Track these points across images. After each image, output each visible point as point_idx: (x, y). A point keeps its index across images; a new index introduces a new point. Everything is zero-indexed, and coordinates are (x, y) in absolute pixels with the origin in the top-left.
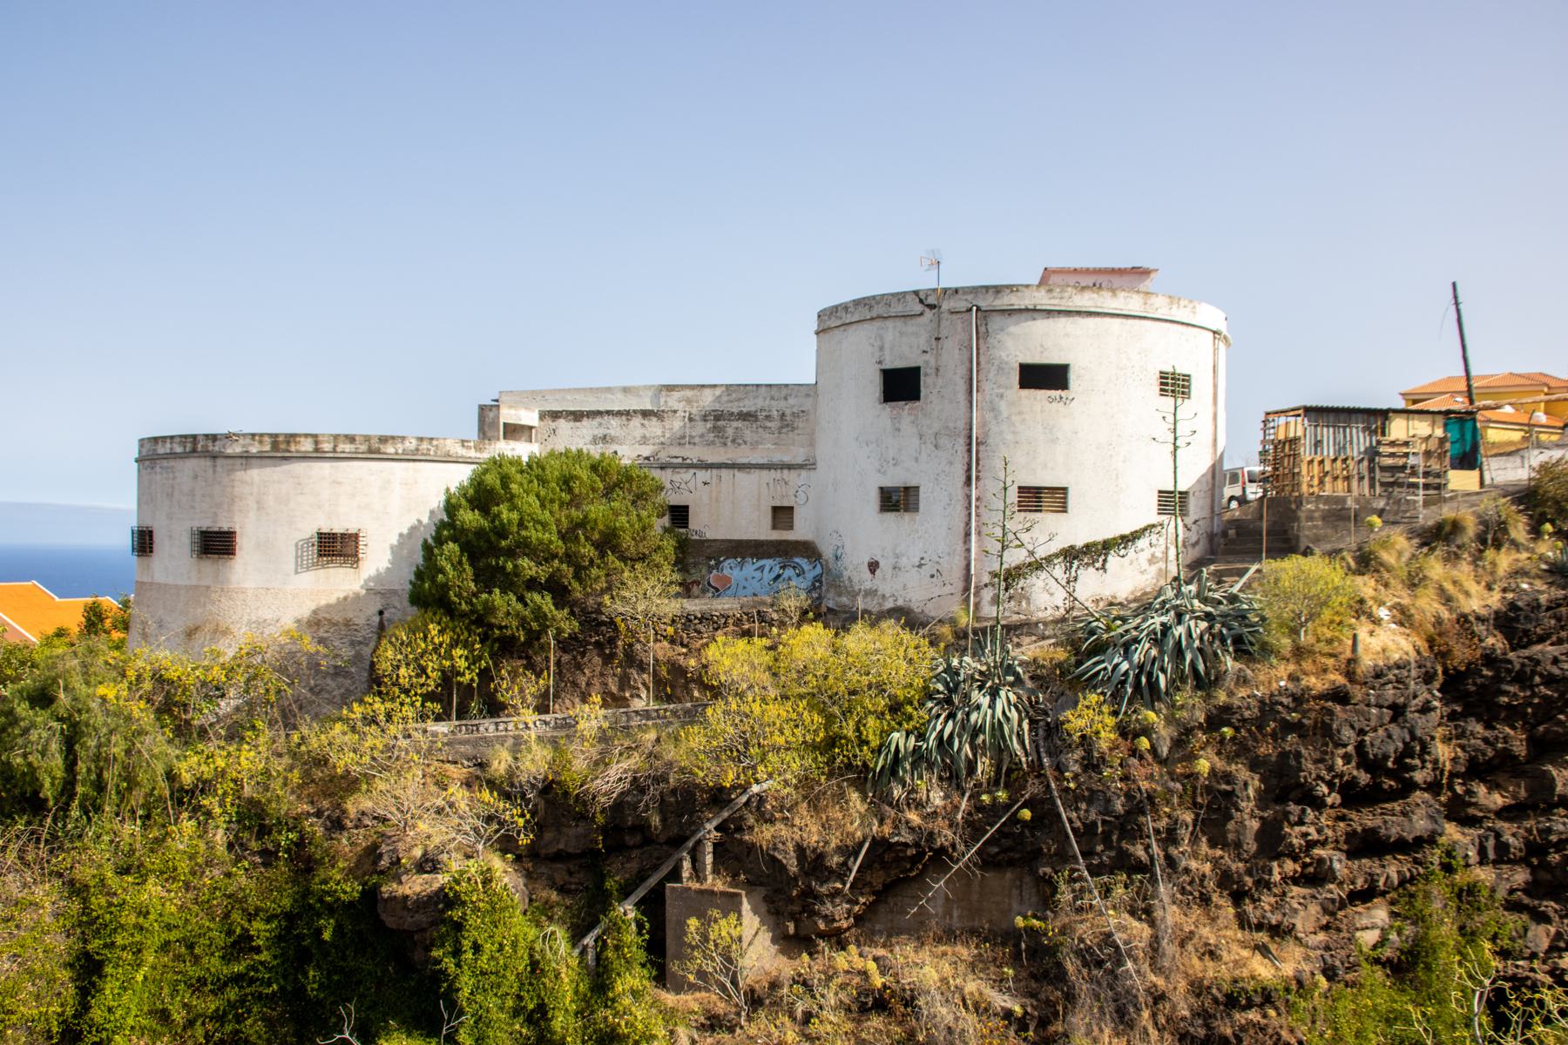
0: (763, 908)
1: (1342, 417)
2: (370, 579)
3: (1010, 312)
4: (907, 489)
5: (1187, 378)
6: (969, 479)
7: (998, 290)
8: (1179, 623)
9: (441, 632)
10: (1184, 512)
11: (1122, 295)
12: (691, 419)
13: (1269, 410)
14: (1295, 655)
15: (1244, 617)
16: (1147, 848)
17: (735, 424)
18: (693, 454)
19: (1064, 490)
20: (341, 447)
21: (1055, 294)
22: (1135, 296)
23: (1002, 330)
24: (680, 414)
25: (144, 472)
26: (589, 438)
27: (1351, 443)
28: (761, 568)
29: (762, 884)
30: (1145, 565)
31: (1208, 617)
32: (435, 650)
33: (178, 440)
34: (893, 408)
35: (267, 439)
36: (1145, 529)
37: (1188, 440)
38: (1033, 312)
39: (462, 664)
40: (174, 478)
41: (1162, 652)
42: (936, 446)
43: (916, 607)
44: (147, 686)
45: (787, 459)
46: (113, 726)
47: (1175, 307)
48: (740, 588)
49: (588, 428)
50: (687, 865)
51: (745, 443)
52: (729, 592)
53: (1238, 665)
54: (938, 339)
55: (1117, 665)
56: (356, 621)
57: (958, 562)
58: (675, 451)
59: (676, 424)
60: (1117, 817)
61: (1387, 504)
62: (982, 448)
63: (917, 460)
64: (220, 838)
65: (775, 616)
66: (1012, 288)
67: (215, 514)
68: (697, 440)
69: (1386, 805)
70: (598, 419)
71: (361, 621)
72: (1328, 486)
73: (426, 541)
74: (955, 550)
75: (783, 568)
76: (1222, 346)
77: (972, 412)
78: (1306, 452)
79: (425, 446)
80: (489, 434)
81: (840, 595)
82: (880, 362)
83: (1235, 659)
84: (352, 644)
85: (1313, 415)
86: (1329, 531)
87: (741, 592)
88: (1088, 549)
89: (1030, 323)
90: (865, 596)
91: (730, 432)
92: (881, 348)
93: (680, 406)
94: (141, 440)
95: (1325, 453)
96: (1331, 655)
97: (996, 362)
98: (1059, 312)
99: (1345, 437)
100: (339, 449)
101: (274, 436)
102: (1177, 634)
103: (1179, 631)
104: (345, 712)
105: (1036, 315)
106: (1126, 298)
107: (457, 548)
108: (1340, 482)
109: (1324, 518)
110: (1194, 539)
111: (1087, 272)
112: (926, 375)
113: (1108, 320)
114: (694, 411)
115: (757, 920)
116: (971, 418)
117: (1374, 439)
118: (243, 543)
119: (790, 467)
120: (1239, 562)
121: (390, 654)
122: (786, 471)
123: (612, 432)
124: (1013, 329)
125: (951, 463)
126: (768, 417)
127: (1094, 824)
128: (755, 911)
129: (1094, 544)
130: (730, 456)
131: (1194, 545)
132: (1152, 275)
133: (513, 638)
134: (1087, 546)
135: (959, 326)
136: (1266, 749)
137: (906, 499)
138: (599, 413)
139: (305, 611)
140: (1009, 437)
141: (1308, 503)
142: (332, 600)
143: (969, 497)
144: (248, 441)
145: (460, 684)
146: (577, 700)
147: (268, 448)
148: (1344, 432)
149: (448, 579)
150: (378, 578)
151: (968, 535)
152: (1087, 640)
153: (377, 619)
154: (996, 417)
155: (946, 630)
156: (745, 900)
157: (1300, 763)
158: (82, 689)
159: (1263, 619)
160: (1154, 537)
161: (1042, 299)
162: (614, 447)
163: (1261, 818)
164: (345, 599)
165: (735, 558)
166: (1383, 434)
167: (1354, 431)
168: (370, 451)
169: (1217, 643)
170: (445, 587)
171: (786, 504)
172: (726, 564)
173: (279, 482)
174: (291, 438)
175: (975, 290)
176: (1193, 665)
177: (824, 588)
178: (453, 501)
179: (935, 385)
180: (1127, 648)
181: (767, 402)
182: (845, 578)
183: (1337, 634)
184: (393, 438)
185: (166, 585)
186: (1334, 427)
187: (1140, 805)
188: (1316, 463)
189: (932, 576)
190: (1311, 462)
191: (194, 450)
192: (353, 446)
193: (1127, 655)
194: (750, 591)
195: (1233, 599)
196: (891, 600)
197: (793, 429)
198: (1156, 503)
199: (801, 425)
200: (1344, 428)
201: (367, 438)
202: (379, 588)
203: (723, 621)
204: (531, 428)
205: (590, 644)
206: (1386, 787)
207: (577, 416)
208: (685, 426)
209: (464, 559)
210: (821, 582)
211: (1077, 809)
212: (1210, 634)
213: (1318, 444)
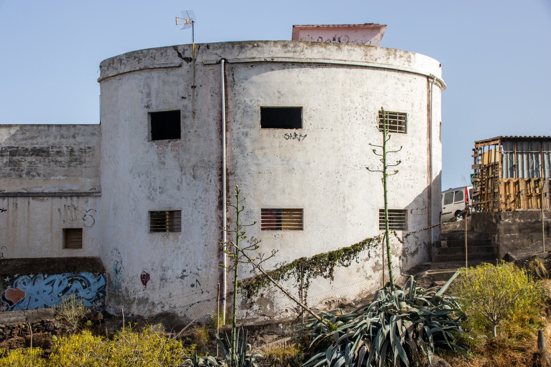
1: (534, 145)
3: (253, 64)
4: (172, 213)
5: (403, 116)
6: (221, 203)
7: (242, 45)
8: (387, 323)
10: (402, 226)
11: (346, 48)
13: (478, 140)
14: (489, 349)
15: (445, 317)
17: (29, 159)
19: (301, 211)
21: (289, 49)
22: (357, 49)
23: (246, 79)
27: (543, 167)
28: (52, 283)
30: (370, 272)
31: (413, 317)
34: (159, 145)
36: (363, 243)
37: (396, 168)
41: (373, 348)
42: (194, 177)
43: (179, 312)
45: (76, 188)
47: (392, 57)
51: (39, 175)
52: (22, 305)
53: (438, 359)
54: (194, 87)
55: (336, 359)
57: (213, 272)
62: (231, 178)
63: (179, 188)
65: (58, 325)
66: (254, 44)
72: (523, 203)
74: (210, 264)
75: (71, 281)
76: (436, 90)
77: (222, 148)
78: (503, 176)
81: (119, 303)
82: (148, 107)
83: (436, 353)
85: (508, 144)
86: (525, 241)
87: (33, 304)
88: (316, 260)
90: (138, 304)
91: (25, 165)
92: (149, 95)
95: (520, 176)
96: (522, 350)
97: (242, 106)
98: (293, 63)
99: (537, 161)
102: (385, 332)
103: (389, 328)
105: (273, 66)
106: (349, 51)
108: (533, 199)
109: (520, 230)
110: (413, 249)
111: (328, 28)
112: (185, 117)
113: (334, 69)
116: (222, 153)
119: (78, 195)
120: (449, 268)
122: (75, 199)
124: (255, 78)
125: (206, 191)
126: (58, 153)
129: (322, 256)
130: (25, 186)
131: (413, 254)
132: (383, 30)
134: (315, 258)
135: (211, 77)
137: (171, 222)
140: (253, 168)
141: (506, 217)
143: (221, 218)
148: (537, 158)
151: (221, 250)
152: (316, 337)
154: (242, 152)
155: (201, 332)
159: (464, 318)
160: (372, 251)
161: (279, 53)
165: (28, 274)
169: (420, 339)
171: (75, 226)
172: (20, 280)
175: (223, 46)
176: (400, 359)
177: (107, 298)
179: (192, 126)
180: (344, 346)
181: (58, 140)
182: (123, 289)
183: (527, 330)
186: (527, 154)
188: (512, 185)
189: (193, 286)
190: (508, 183)
193: (344, 351)
194: (41, 303)
195: (436, 300)
196: (159, 306)
197: (81, 163)
198: (379, 216)
200: (537, 155)
203: (8, 332)
210: (104, 293)
212: (415, 331)
213: (513, 168)
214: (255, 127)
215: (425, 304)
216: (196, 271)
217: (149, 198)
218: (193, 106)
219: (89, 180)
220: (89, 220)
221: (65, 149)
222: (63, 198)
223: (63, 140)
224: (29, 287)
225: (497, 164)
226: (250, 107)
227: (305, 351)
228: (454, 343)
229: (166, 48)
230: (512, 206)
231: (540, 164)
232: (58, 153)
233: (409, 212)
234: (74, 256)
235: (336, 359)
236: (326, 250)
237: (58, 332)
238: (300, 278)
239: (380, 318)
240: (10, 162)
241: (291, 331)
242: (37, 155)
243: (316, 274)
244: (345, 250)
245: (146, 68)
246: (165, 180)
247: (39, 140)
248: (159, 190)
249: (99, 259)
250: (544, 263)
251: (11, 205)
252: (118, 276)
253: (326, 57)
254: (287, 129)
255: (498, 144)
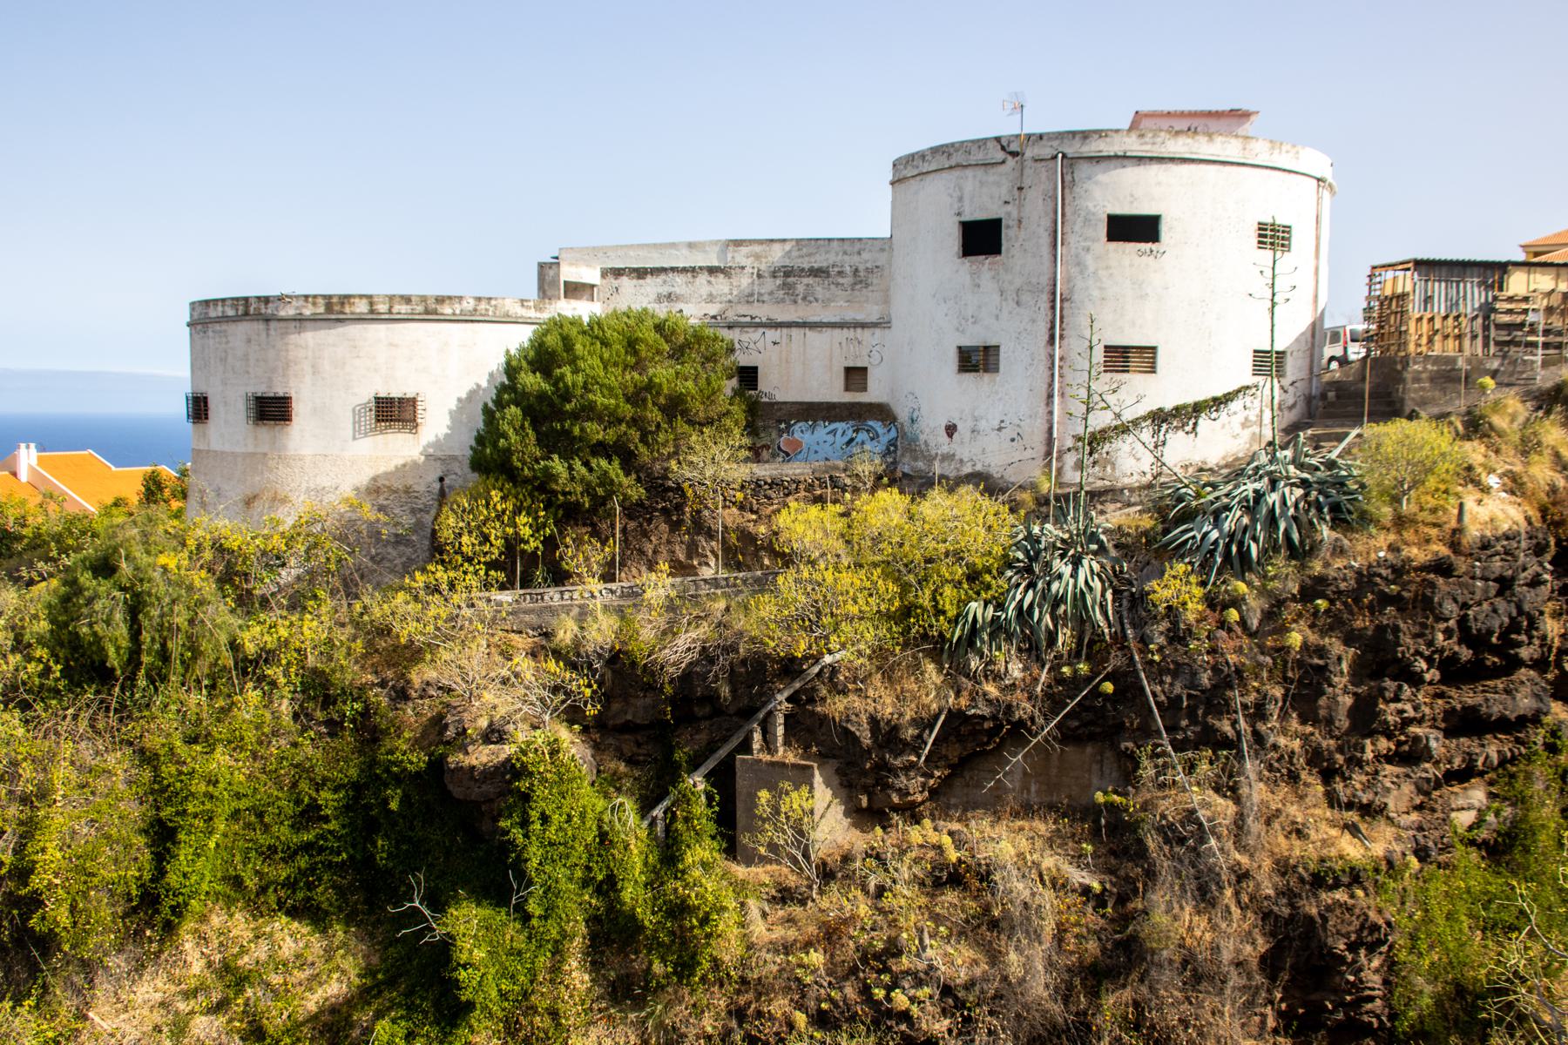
0: (836, 780)
1: (1456, 271)
2: (429, 445)
3: (1098, 159)
4: (986, 348)
7: (1085, 135)
8: (1273, 489)
9: (504, 498)
12: (759, 276)
16: (1234, 723)
17: (805, 280)
18: (763, 312)
20: (396, 308)
21: (1147, 139)
23: (1089, 178)
24: (748, 270)
25: (196, 337)
26: (653, 297)
27: (1465, 299)
28: (834, 432)
29: (834, 757)
30: (1238, 429)
31: (1304, 483)
32: (499, 517)
33: (227, 303)
35: (321, 301)
36: (1239, 391)
38: (1123, 159)
39: (526, 532)
40: (227, 342)
41: (1254, 521)
42: (1018, 303)
43: (995, 472)
44: (208, 555)
45: (861, 317)
46: (175, 596)
48: (812, 452)
49: (652, 286)
50: (757, 736)
51: (817, 300)
52: (799, 457)
53: (1334, 535)
54: (1020, 189)
55: (1206, 534)
56: (416, 488)
57: (1040, 426)
58: (743, 309)
59: (744, 281)
60: (1203, 692)
61: (1502, 365)
62: (1066, 305)
63: (997, 317)
64: (285, 707)
65: (848, 481)
67: (270, 379)
68: (766, 298)
69: (1488, 683)
70: (663, 277)
71: (422, 488)
73: (486, 405)
75: (856, 431)
76: (1326, 194)
78: (1414, 309)
79: (483, 306)
80: (549, 293)
81: (916, 459)
82: (959, 214)
83: (1332, 528)
84: (413, 511)
85: (1424, 268)
86: (1437, 394)
87: (812, 456)
88: (1178, 411)
89: (1120, 171)
91: (800, 289)
92: (961, 199)
93: (748, 262)
94: (192, 304)
95: (1436, 310)
98: (1151, 159)
99: (1458, 292)
100: (394, 311)
101: (328, 298)
102: (1270, 501)
104: (407, 581)
105: (1126, 162)
106: (1223, 143)
107: (519, 412)
109: (1432, 380)
110: (1290, 402)
111: (1182, 115)
112: (1008, 227)
113: (1203, 167)
114: (763, 267)
115: (829, 792)
116: (1055, 273)
117: (1490, 294)
118: (299, 409)
120: (1338, 426)
121: (451, 521)
122: (859, 330)
123: (677, 290)
124: (1102, 177)
125: (1034, 321)
126: (840, 273)
127: (1179, 697)
128: (828, 784)
129: (1185, 407)
130: (801, 313)
131: (1291, 408)
132: (1253, 118)
133: (578, 504)
134: (1177, 409)
135: (1044, 175)
136: (1361, 622)
138: (663, 270)
139: (363, 477)
140: (1096, 293)
141: (1415, 363)
142: (391, 467)
143: (1052, 357)
144: (301, 302)
145: (523, 552)
146: (644, 568)
147: (321, 310)
148: (1458, 287)
149: (510, 444)
150: (437, 444)
151: (1050, 396)
152: (1175, 507)
153: (437, 486)
154: (1081, 272)
156: (817, 773)
157: (1398, 637)
158: (144, 559)
159: (1363, 486)
160: (1248, 399)
161: (1133, 145)
162: (680, 306)
163: (1355, 694)
164: (404, 465)
166: (1501, 289)
167: (1469, 285)
168: (427, 312)
169: (1313, 511)
170: (508, 452)
171: (859, 364)
172: (796, 427)
173: (334, 345)
174: (346, 299)
176: (1287, 533)
177: (899, 453)
178: (514, 363)
179: (1017, 237)
180: (1217, 517)
181: (840, 257)
182: (922, 442)
183: (1441, 502)
184: (450, 298)
185: (222, 453)
186: (1446, 281)
187: (1227, 679)
188: (1425, 321)
189: (1013, 440)
190: (1420, 319)
191: (246, 314)
192: (409, 307)
193: (1217, 523)
194: (821, 455)
195: (1331, 465)
196: (969, 464)
197: (867, 285)
199: (875, 281)
201: (424, 299)
202: (439, 454)
203: (794, 486)
204: (593, 286)
205: (656, 510)
206: (1488, 663)
207: (641, 273)
208: (753, 283)
209: (526, 424)
210: (896, 447)
211: (1162, 683)
213: (1428, 300)
214: (1099, 240)
215: (1317, 469)
216: (1016, 421)
217: (958, 329)
218: (1019, 212)
219: (876, 307)
220: (876, 357)
221: (848, 268)
222: (845, 330)
223: (846, 258)
224: (807, 435)
225: (1408, 294)
226: (1094, 214)
227: (1162, 523)
228: (1354, 517)
229: (986, 139)
230: (1424, 349)
231: (1461, 294)
232: (840, 273)
233: (1288, 354)
234: (857, 400)
235: (1206, 534)
236: (1190, 399)
237: (849, 489)
238: (1156, 433)
239: (1263, 484)
240: (784, 284)
241: (1138, 499)
242: (816, 276)
243: (1177, 428)
244: (1215, 399)
245: (958, 166)
246: (980, 307)
247: (818, 257)
248: (971, 320)
249: (888, 405)
250: (1462, 422)
251: (784, 337)
252: (915, 426)
253: (1194, 150)
254: (1148, 242)
255: (1408, 269)
